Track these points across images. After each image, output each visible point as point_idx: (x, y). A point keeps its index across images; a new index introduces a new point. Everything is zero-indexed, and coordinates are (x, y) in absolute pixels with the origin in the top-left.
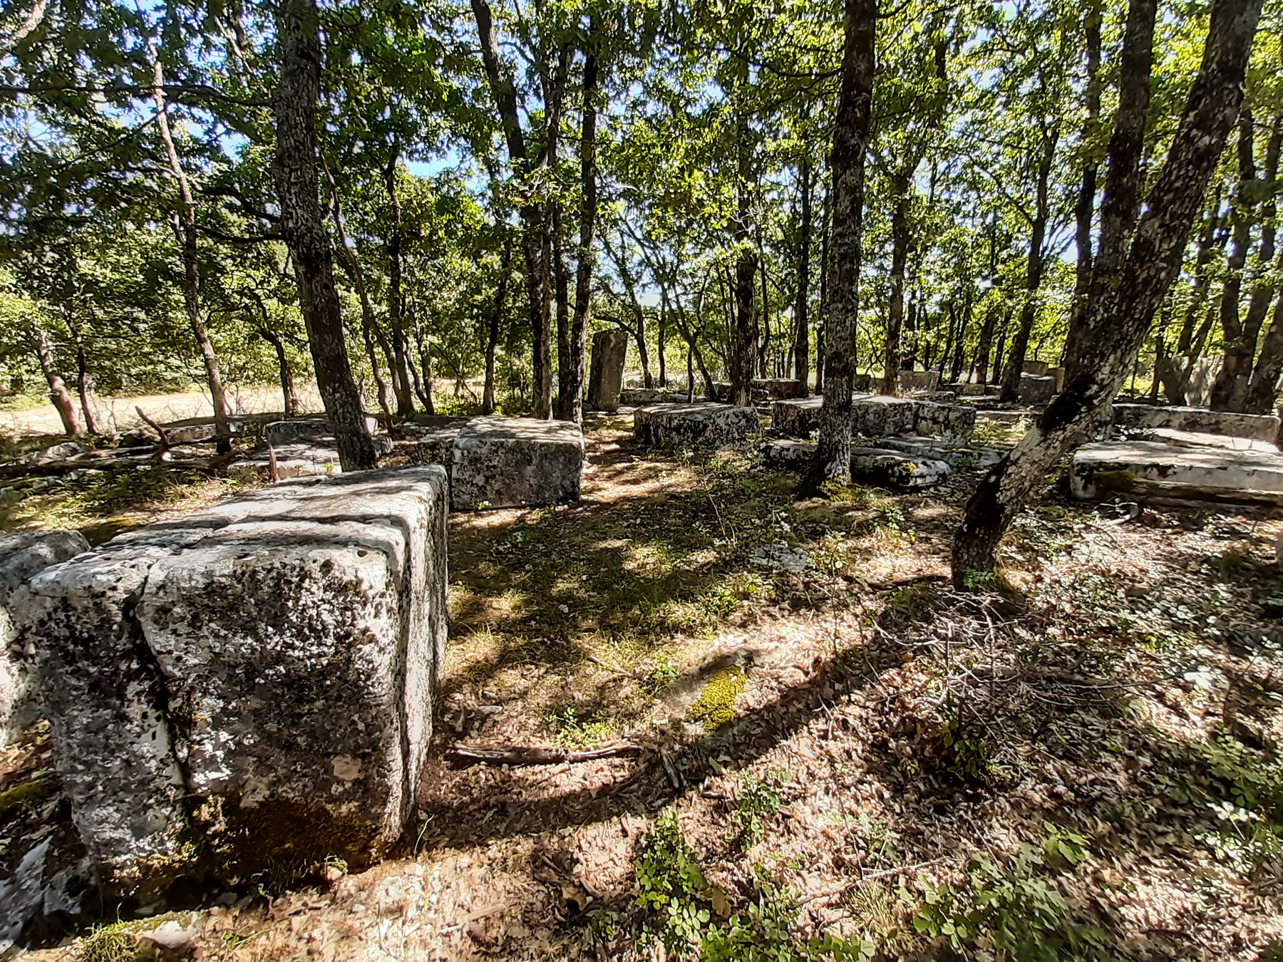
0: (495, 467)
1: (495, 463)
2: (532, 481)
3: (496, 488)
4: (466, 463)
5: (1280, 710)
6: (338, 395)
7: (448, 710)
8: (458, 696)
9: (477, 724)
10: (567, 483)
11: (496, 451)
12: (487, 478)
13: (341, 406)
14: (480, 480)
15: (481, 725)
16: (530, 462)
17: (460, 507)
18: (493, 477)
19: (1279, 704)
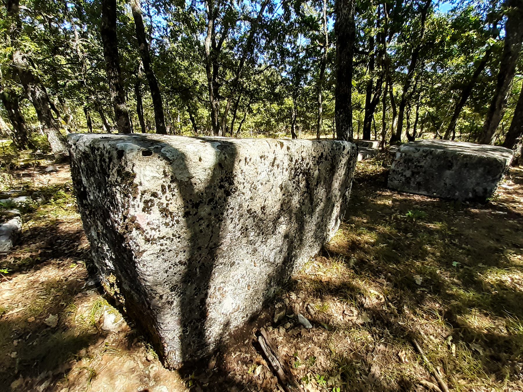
0: (421, 167)
1: (422, 164)
2: (447, 181)
3: (418, 180)
4: (402, 161)
5: (516, 258)
6: (341, 116)
7: (281, 300)
8: (293, 296)
9: (288, 325)
10: (480, 189)
11: (425, 156)
12: (413, 173)
13: (342, 122)
14: (408, 173)
15: (291, 328)
16: (450, 167)
17: (391, 187)
18: (418, 173)
19: (3, 158)
